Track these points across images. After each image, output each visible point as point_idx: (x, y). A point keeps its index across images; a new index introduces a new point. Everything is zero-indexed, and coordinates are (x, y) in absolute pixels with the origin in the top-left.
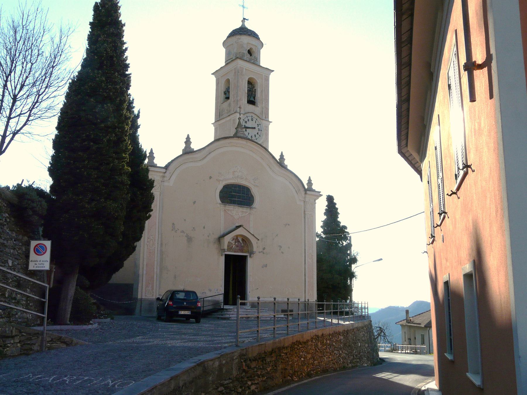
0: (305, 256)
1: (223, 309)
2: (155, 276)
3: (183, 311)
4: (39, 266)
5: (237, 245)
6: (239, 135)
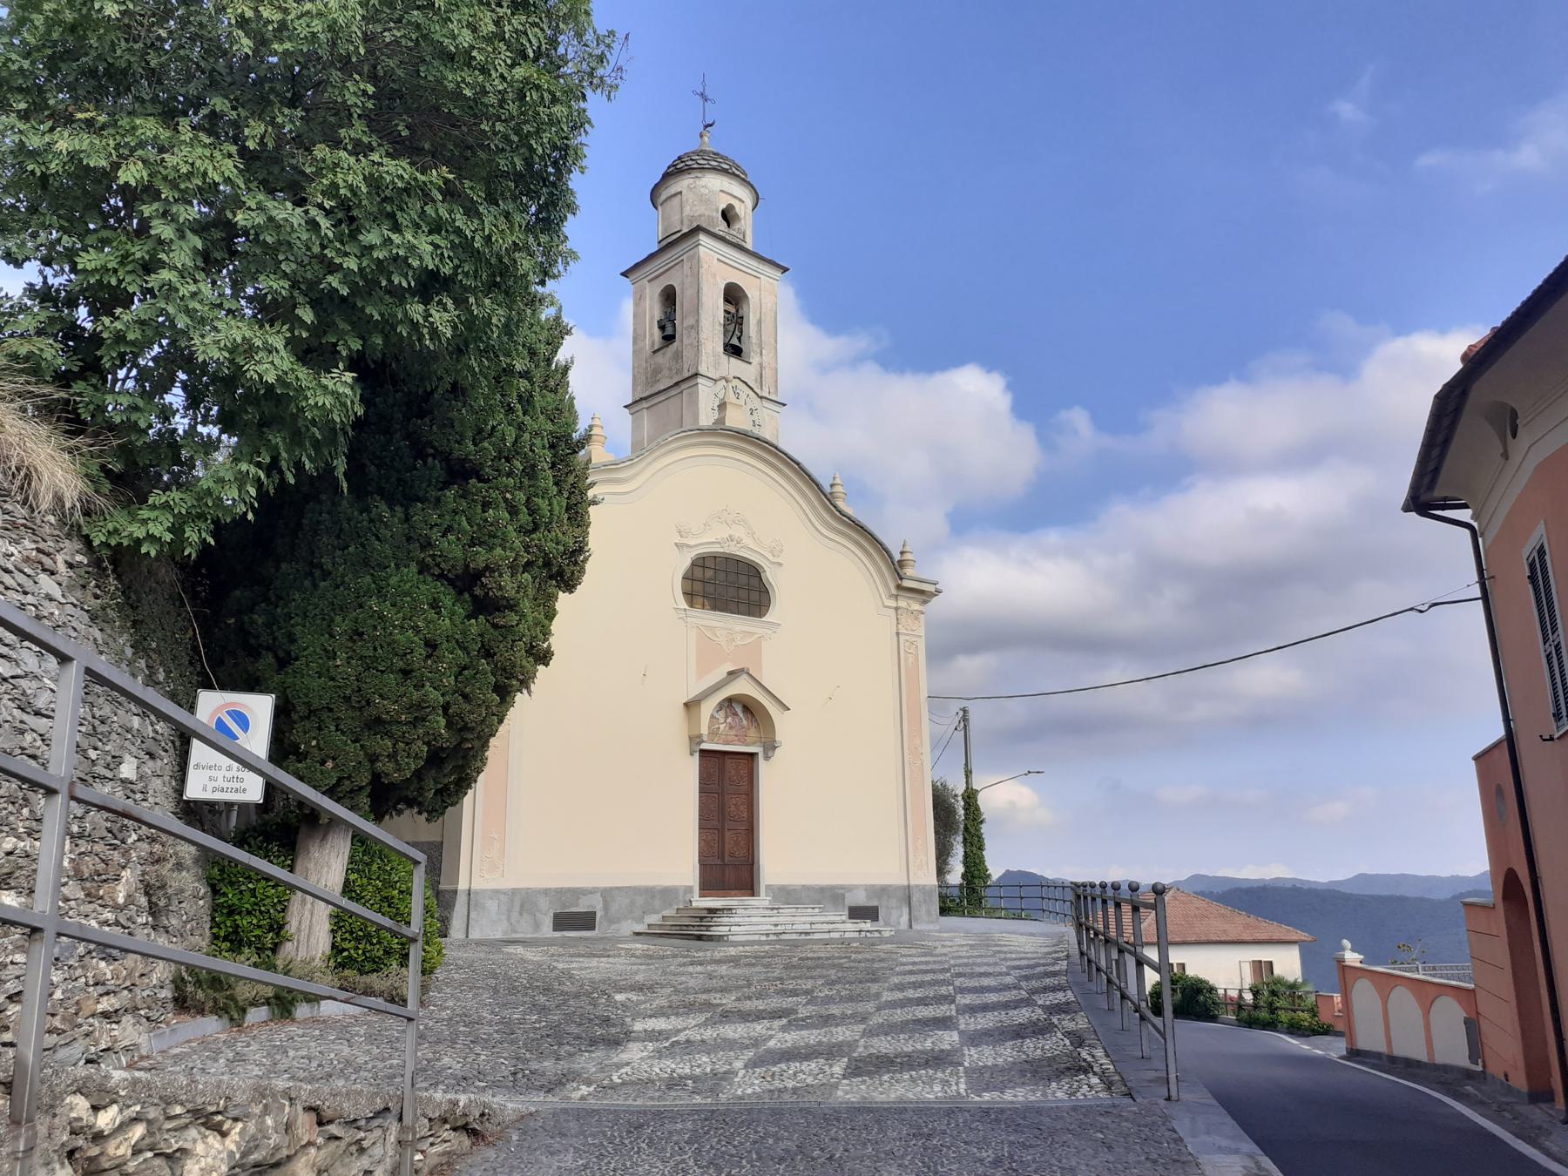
4: (225, 785)
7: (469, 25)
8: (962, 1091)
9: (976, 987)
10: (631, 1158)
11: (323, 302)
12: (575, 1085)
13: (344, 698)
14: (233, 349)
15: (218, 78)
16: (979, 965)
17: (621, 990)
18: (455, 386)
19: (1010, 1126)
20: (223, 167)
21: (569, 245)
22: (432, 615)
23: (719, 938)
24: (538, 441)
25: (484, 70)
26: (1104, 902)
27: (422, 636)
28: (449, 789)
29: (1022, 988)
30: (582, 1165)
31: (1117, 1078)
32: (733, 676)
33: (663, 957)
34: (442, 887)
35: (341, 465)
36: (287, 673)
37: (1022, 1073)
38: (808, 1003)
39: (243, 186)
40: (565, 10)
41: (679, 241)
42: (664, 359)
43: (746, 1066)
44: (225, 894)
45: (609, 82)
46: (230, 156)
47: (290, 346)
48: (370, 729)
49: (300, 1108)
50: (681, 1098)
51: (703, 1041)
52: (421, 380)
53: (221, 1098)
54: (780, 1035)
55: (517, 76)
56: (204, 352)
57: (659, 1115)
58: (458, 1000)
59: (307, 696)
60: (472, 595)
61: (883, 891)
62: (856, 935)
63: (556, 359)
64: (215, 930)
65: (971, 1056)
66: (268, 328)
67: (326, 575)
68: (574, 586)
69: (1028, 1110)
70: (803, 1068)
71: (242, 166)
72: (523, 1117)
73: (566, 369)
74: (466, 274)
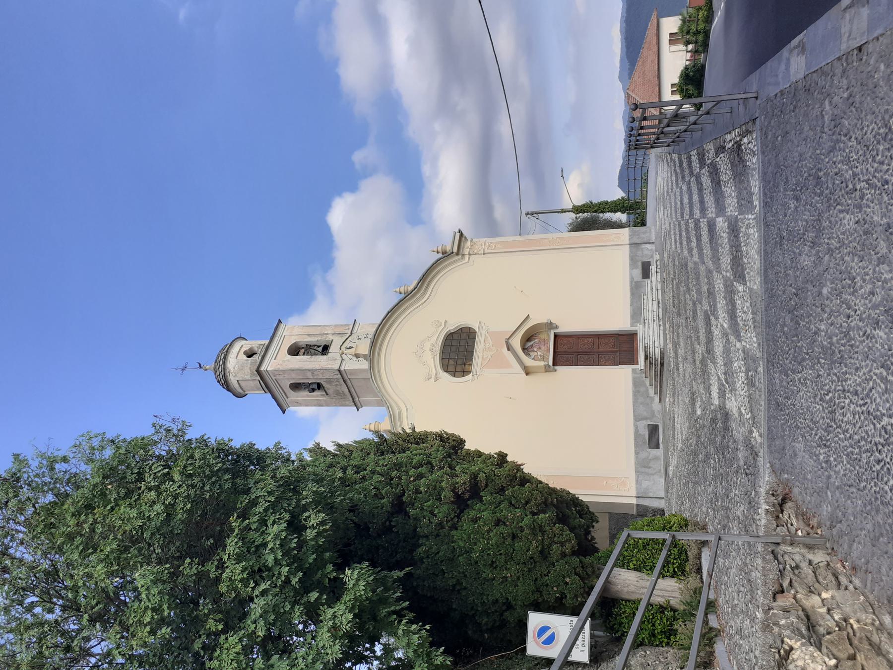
7: (151, 506)
8: (753, 217)
9: (689, 207)
10: (798, 410)
11: (306, 587)
12: (753, 440)
13: (529, 572)
14: (334, 637)
15: (183, 645)
16: (676, 204)
17: (694, 411)
18: (350, 511)
19: (775, 190)
20: (233, 642)
21: (271, 447)
22: (480, 522)
23: (662, 353)
24: (381, 462)
25: (176, 497)
26: (639, 135)
27: (493, 528)
28: (579, 510)
29: (690, 180)
30: (802, 438)
31: (744, 127)
32: (510, 348)
33: (674, 386)
34: (635, 513)
35: (397, 574)
36: (515, 605)
37: (741, 182)
38: (701, 303)
39: (243, 632)
40: (142, 452)
41: (265, 382)
42: (331, 389)
43: (740, 341)
44: (643, 639)
45: (181, 426)
46: (227, 639)
47: (332, 605)
48: (547, 557)
49: (774, 604)
50: (760, 379)
51: (725, 365)
52: (348, 530)
53: (771, 651)
54: (720, 320)
55: (179, 479)
56: (336, 654)
57: (771, 392)
58: (702, 505)
59: (529, 593)
60: (468, 500)
61: (633, 259)
62: (659, 274)
63: (333, 451)
64: (664, 644)
65: (731, 211)
66: (322, 618)
67: (459, 583)
68: (461, 439)
69: (764, 179)
70: (740, 308)
71: (232, 632)
72: (773, 471)
73: (339, 445)
74: (289, 505)
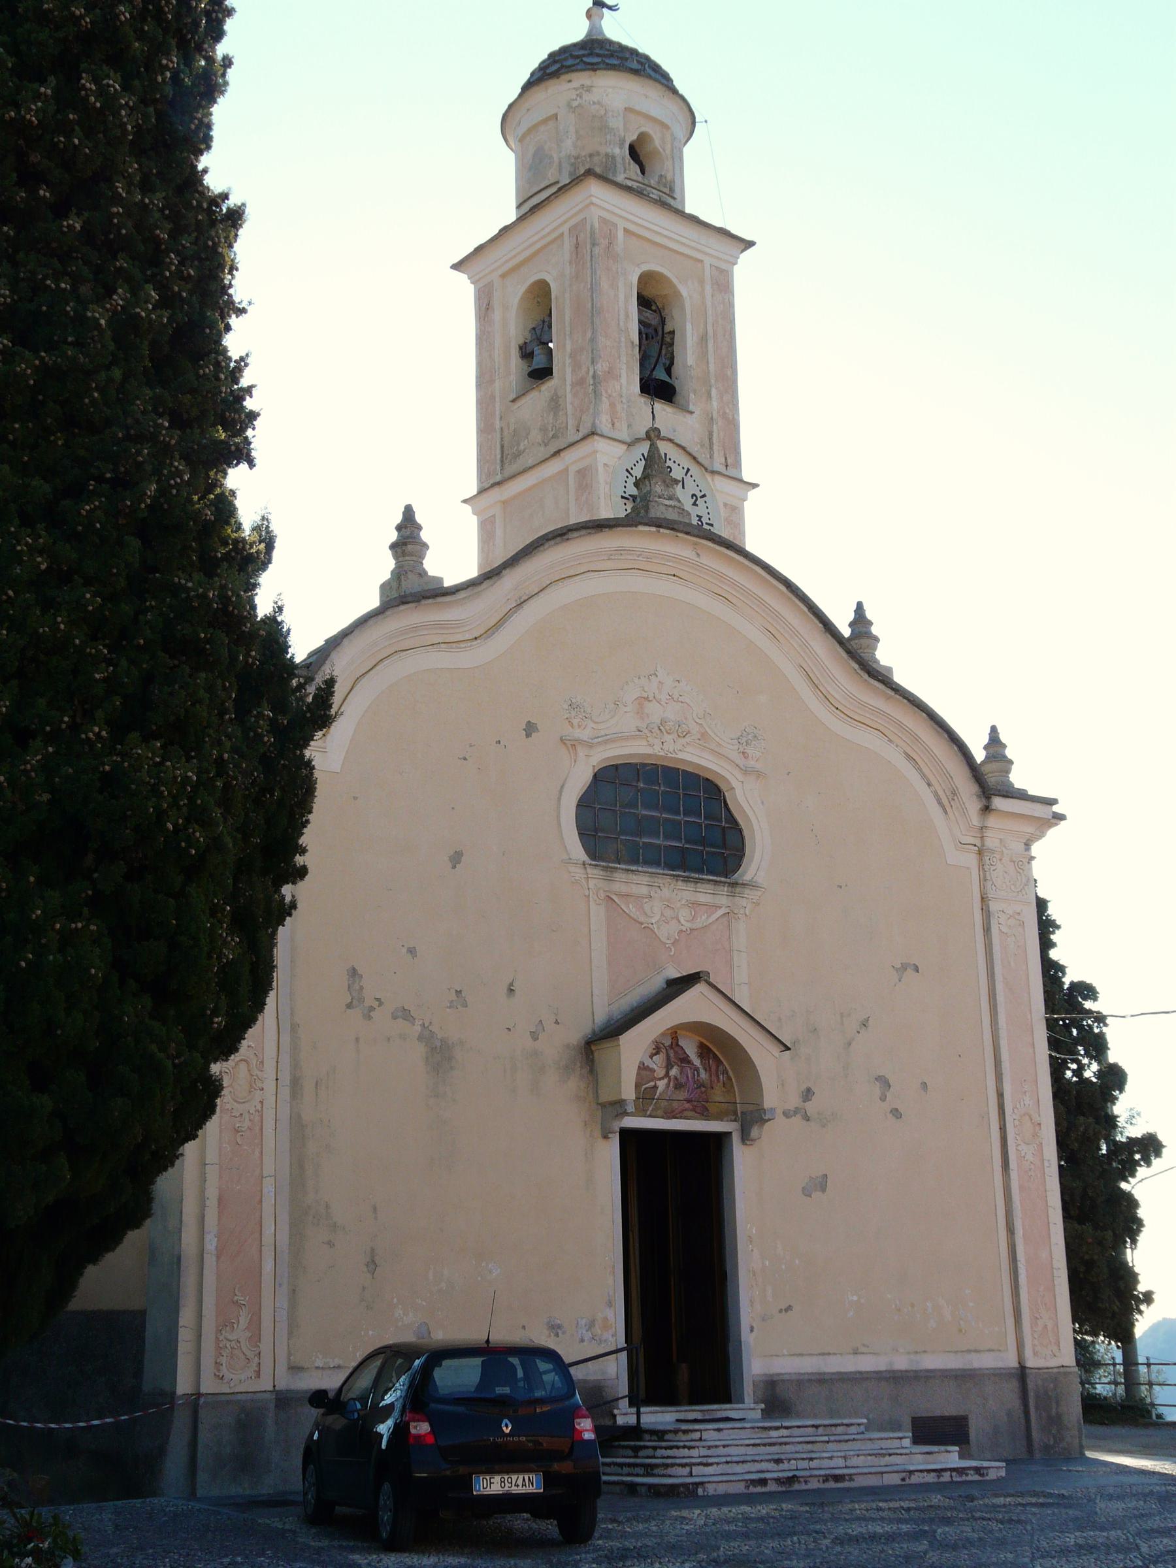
0: (1003, 1129)
1: (636, 1431)
2: (268, 1266)
3: (499, 1472)
5: (676, 1078)
6: (657, 512)
23: (673, 1494)
